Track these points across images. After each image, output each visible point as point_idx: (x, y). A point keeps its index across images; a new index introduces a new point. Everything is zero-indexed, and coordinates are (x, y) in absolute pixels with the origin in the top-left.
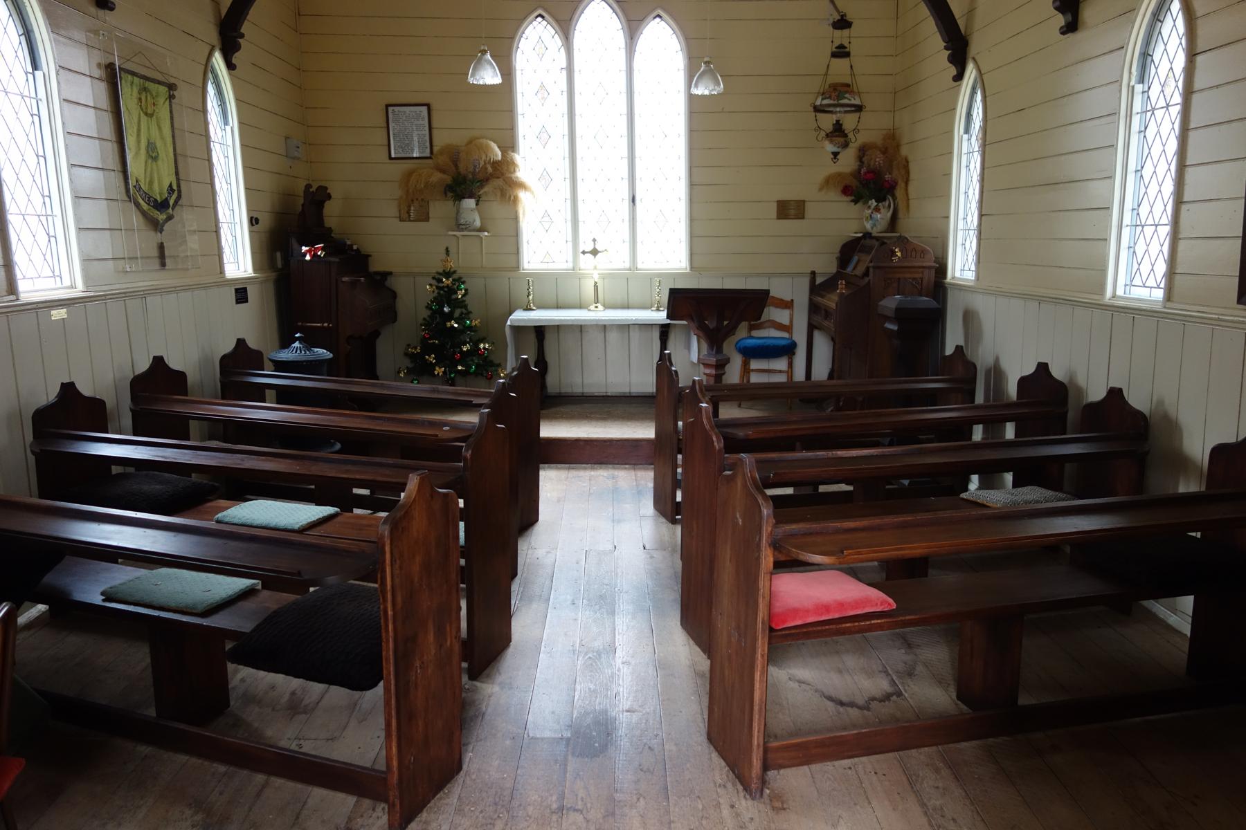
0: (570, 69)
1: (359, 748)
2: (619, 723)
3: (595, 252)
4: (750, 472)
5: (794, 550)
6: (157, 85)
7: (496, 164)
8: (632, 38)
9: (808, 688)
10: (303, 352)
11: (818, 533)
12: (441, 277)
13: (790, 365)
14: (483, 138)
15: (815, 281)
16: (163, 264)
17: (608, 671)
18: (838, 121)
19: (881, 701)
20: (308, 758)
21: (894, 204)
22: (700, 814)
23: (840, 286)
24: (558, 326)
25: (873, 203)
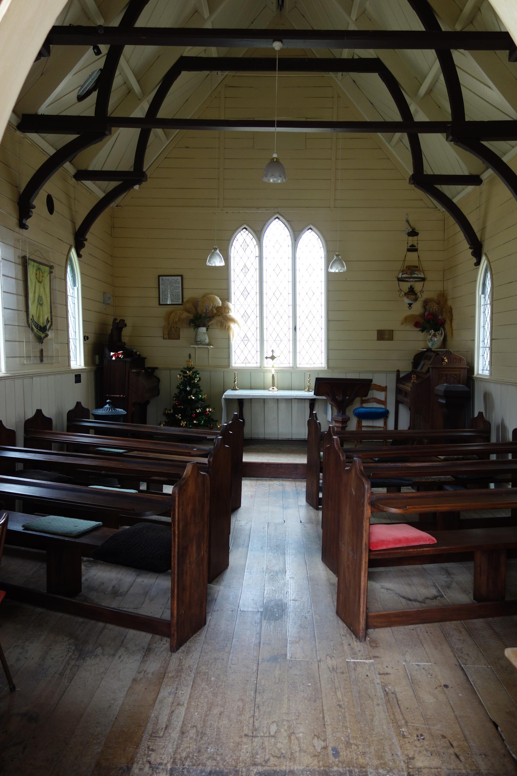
0: (261, 257)
1: (151, 613)
2: (289, 606)
3: (273, 358)
4: (359, 466)
5: (381, 506)
6: (44, 267)
7: (218, 308)
8: (295, 241)
9: (392, 592)
10: (111, 410)
11: (393, 499)
12: (186, 370)
13: (385, 424)
14: (211, 294)
15: (399, 375)
16: (42, 360)
17: (282, 582)
18: (411, 286)
19: (431, 599)
20: (127, 613)
21: (445, 333)
22: (332, 648)
23: (413, 378)
24: (251, 399)
25: (432, 332)
